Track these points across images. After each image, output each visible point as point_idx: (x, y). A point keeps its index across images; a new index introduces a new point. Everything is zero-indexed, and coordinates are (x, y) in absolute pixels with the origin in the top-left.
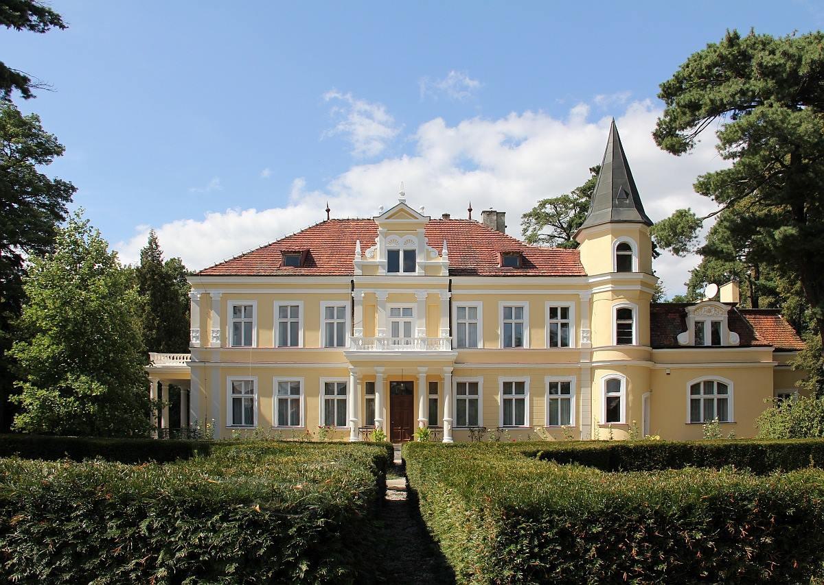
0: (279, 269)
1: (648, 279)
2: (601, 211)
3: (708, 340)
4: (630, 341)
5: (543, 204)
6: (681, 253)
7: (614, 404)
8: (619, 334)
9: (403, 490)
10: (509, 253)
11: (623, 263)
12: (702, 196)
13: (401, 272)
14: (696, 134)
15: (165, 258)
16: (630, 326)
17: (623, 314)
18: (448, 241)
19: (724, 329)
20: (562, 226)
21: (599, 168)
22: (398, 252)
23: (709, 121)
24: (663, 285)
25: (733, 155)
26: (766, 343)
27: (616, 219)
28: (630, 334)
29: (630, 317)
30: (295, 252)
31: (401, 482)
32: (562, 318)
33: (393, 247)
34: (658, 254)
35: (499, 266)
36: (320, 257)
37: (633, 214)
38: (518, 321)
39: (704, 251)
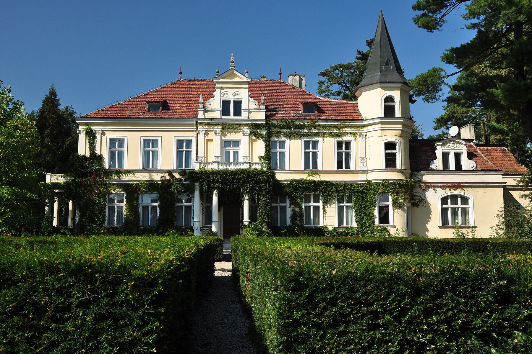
0: (144, 113)
1: (408, 123)
2: (373, 73)
3: (452, 166)
4: (395, 166)
5: (334, 68)
6: (431, 101)
7: (384, 211)
8: (387, 160)
9: (229, 271)
10: (308, 103)
11: (389, 111)
12: (448, 64)
13: (232, 117)
14: (443, 16)
15: (62, 107)
16: (394, 155)
17: (390, 146)
18: (265, 95)
19: (464, 158)
20: (346, 85)
21: (372, 41)
22: (229, 102)
23: (453, 7)
24: (437, 30)
25: (474, 26)
26: (496, 168)
27: (383, 79)
28: (395, 160)
29: (394, 149)
30: (156, 102)
31: (228, 265)
32: (345, 149)
33: (226, 98)
34: (415, 101)
35: (301, 112)
36: (176, 107)
37: (396, 76)
38: (281, 150)
39: (450, 100)
